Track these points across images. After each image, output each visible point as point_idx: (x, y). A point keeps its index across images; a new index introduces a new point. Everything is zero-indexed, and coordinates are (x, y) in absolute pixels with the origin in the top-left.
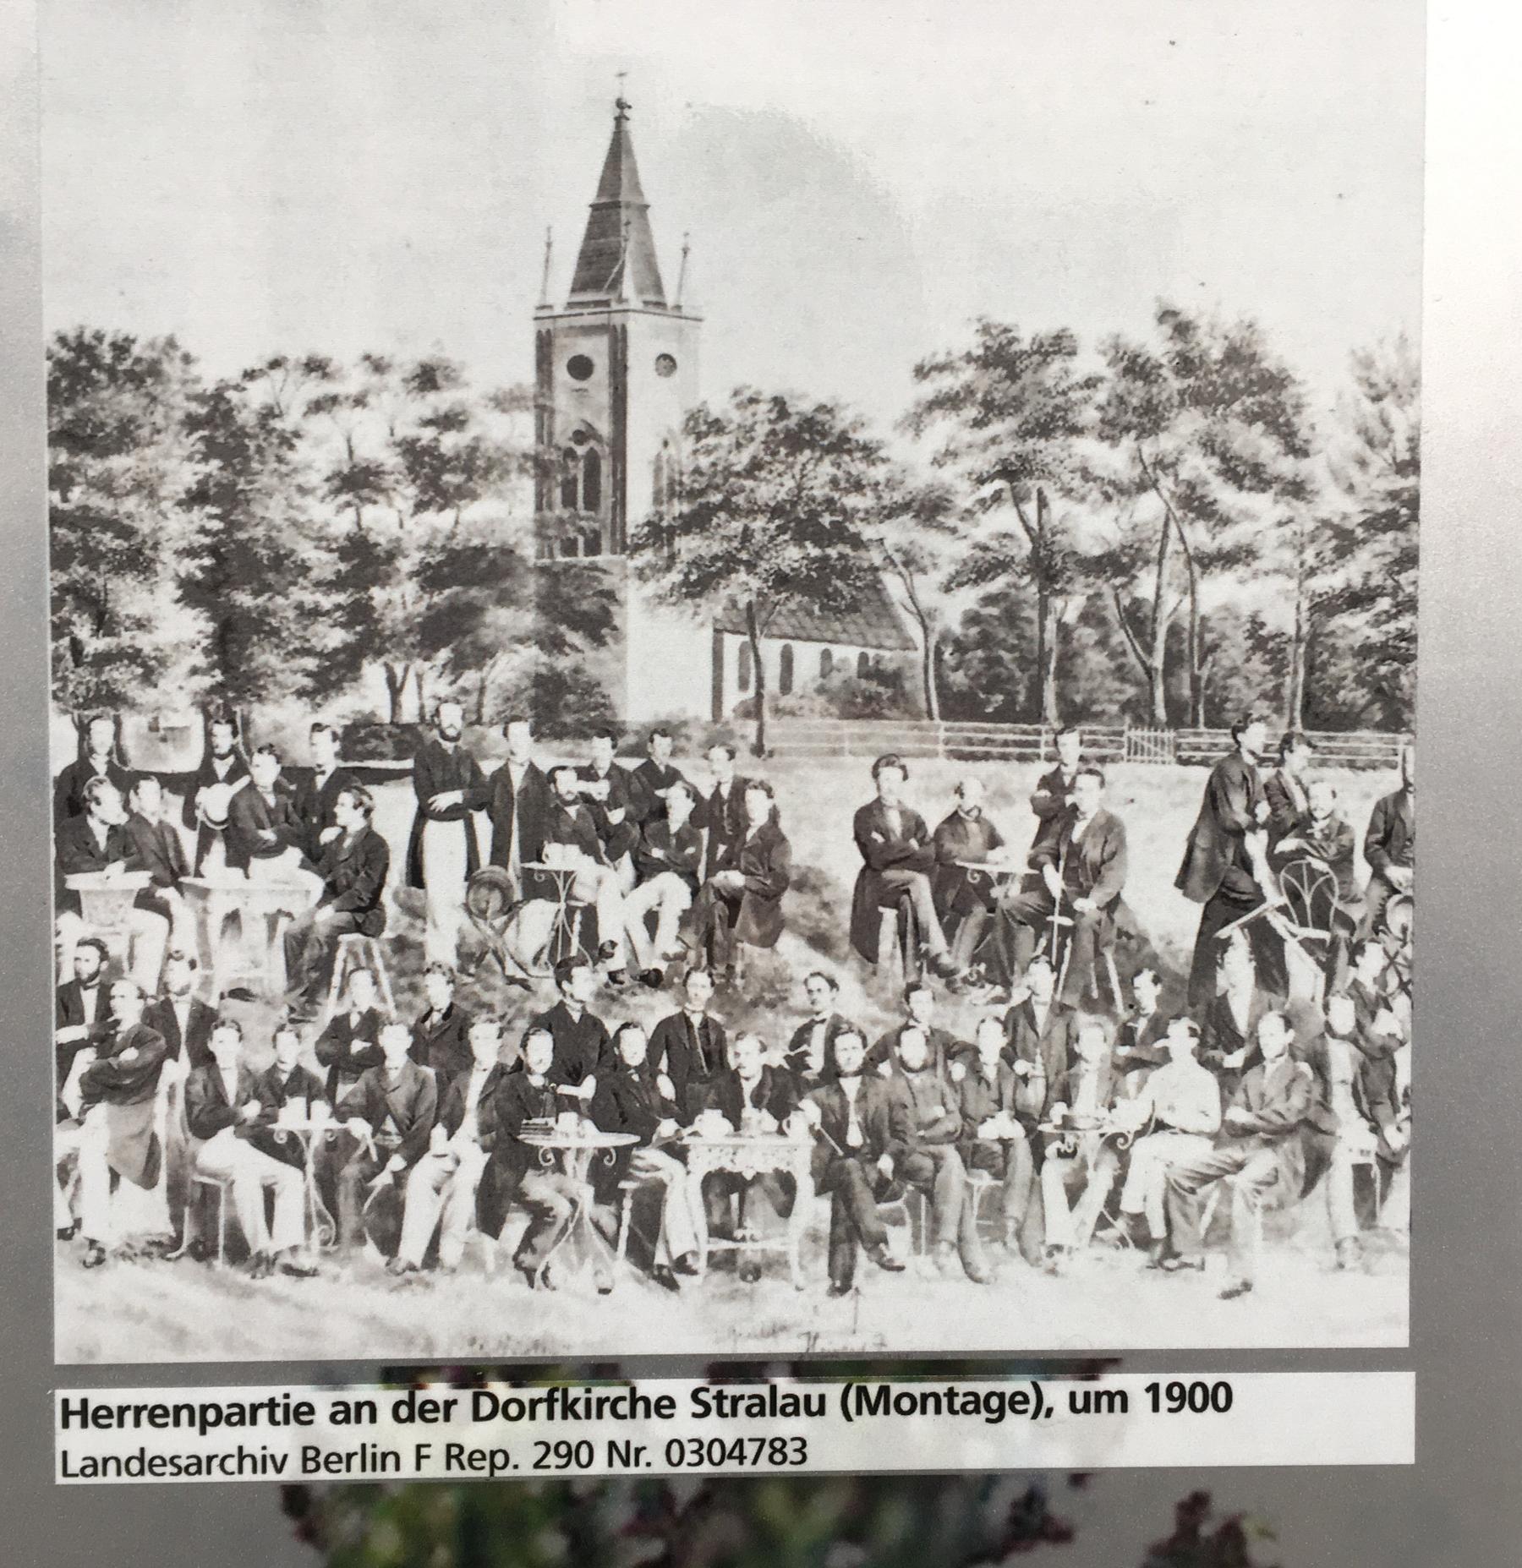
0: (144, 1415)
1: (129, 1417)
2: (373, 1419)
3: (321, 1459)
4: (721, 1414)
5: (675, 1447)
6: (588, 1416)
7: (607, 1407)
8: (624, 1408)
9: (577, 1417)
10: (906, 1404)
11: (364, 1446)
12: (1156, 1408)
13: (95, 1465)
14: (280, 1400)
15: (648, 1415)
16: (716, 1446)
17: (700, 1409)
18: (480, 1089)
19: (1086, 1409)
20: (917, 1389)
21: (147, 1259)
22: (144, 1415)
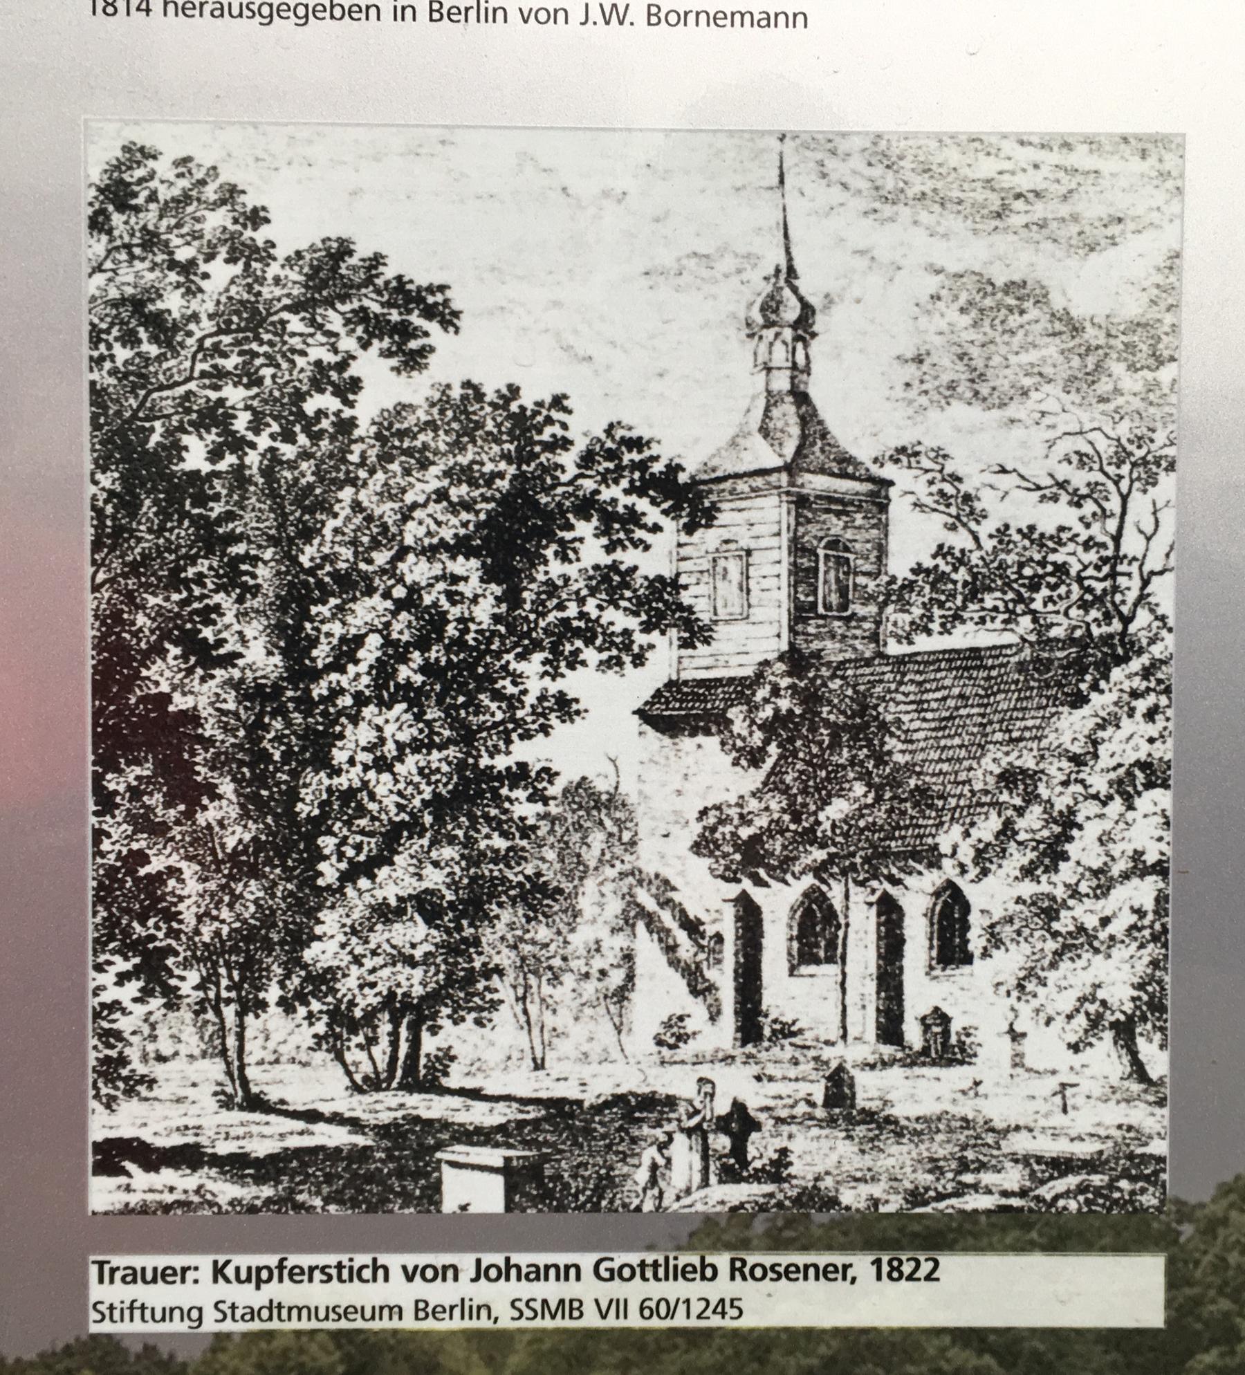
2: (578, 1278)
3: (429, 1310)
6: (667, 1278)
8: (367, 1274)
9: (227, 1281)
10: (758, 1272)
12: (879, 1278)
14: (346, 1263)
15: (817, 1278)
16: (663, 1304)
18: (908, 949)
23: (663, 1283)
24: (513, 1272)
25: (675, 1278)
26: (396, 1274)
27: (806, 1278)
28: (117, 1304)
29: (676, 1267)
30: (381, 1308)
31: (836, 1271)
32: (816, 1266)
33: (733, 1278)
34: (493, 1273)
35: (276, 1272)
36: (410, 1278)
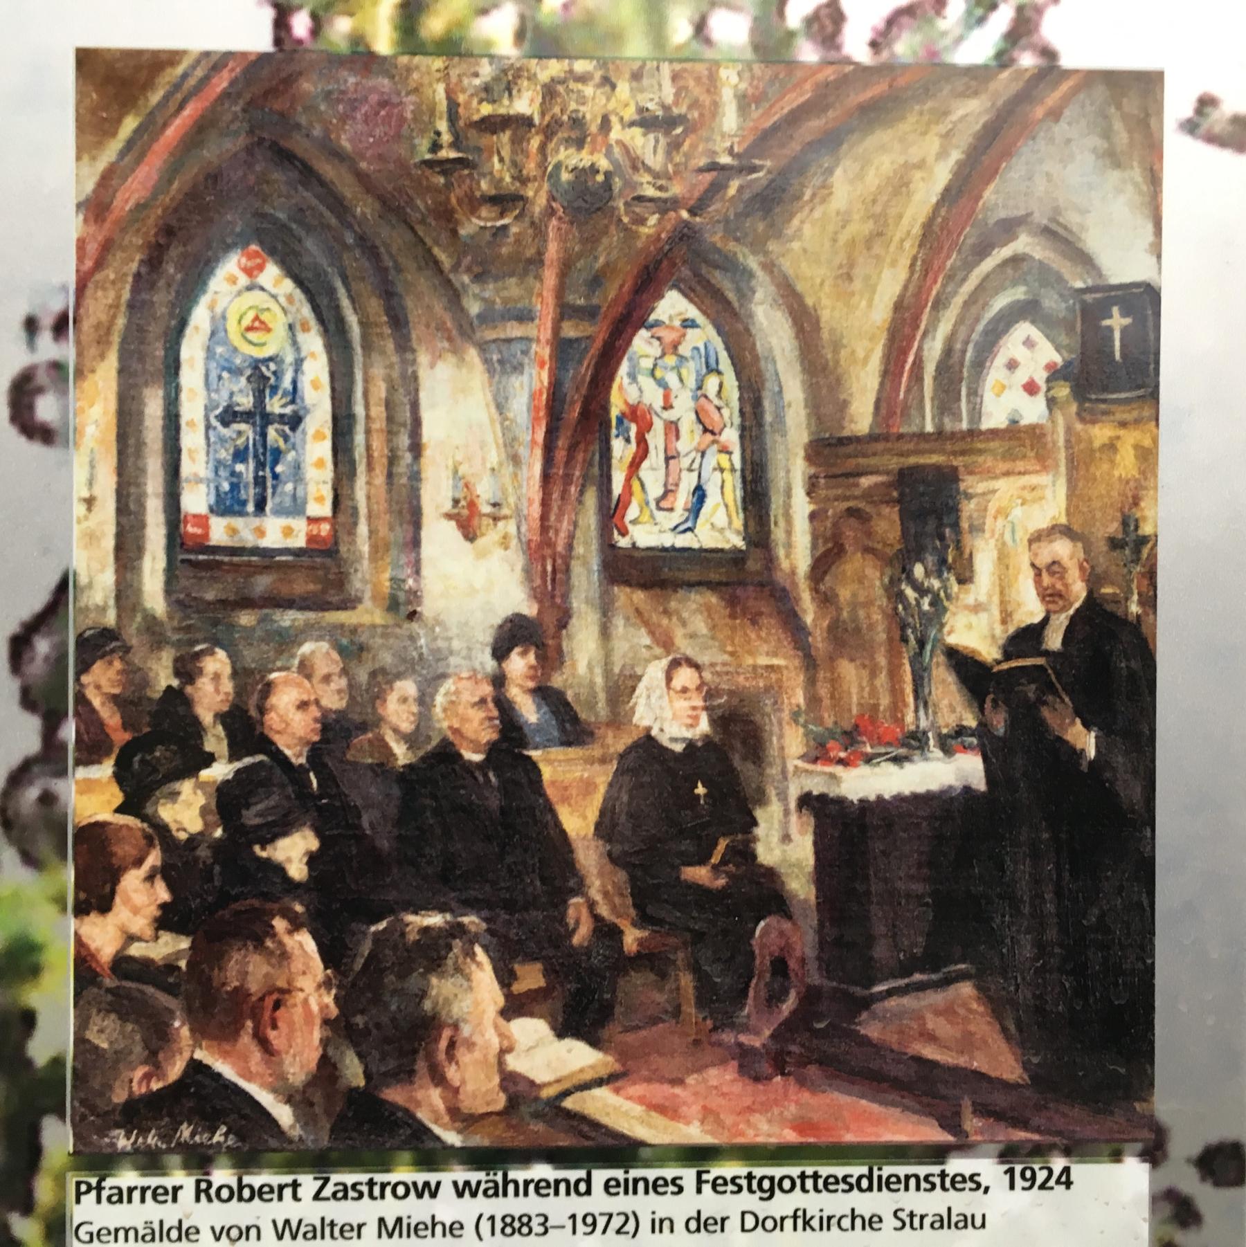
0: (149, 1194)
1: (136, 1195)
12: (1012, 1187)
15: (647, 1192)
20: (902, 1170)
21: (282, 1009)
22: (149, 1194)
23: (379, 1201)
24: (511, 1187)
25: (880, 1189)
26: (447, 1191)
29: (880, 1177)
31: (899, 1181)
32: (646, 1180)
33: (198, 1199)
34: (225, 1193)
36: (460, 1194)
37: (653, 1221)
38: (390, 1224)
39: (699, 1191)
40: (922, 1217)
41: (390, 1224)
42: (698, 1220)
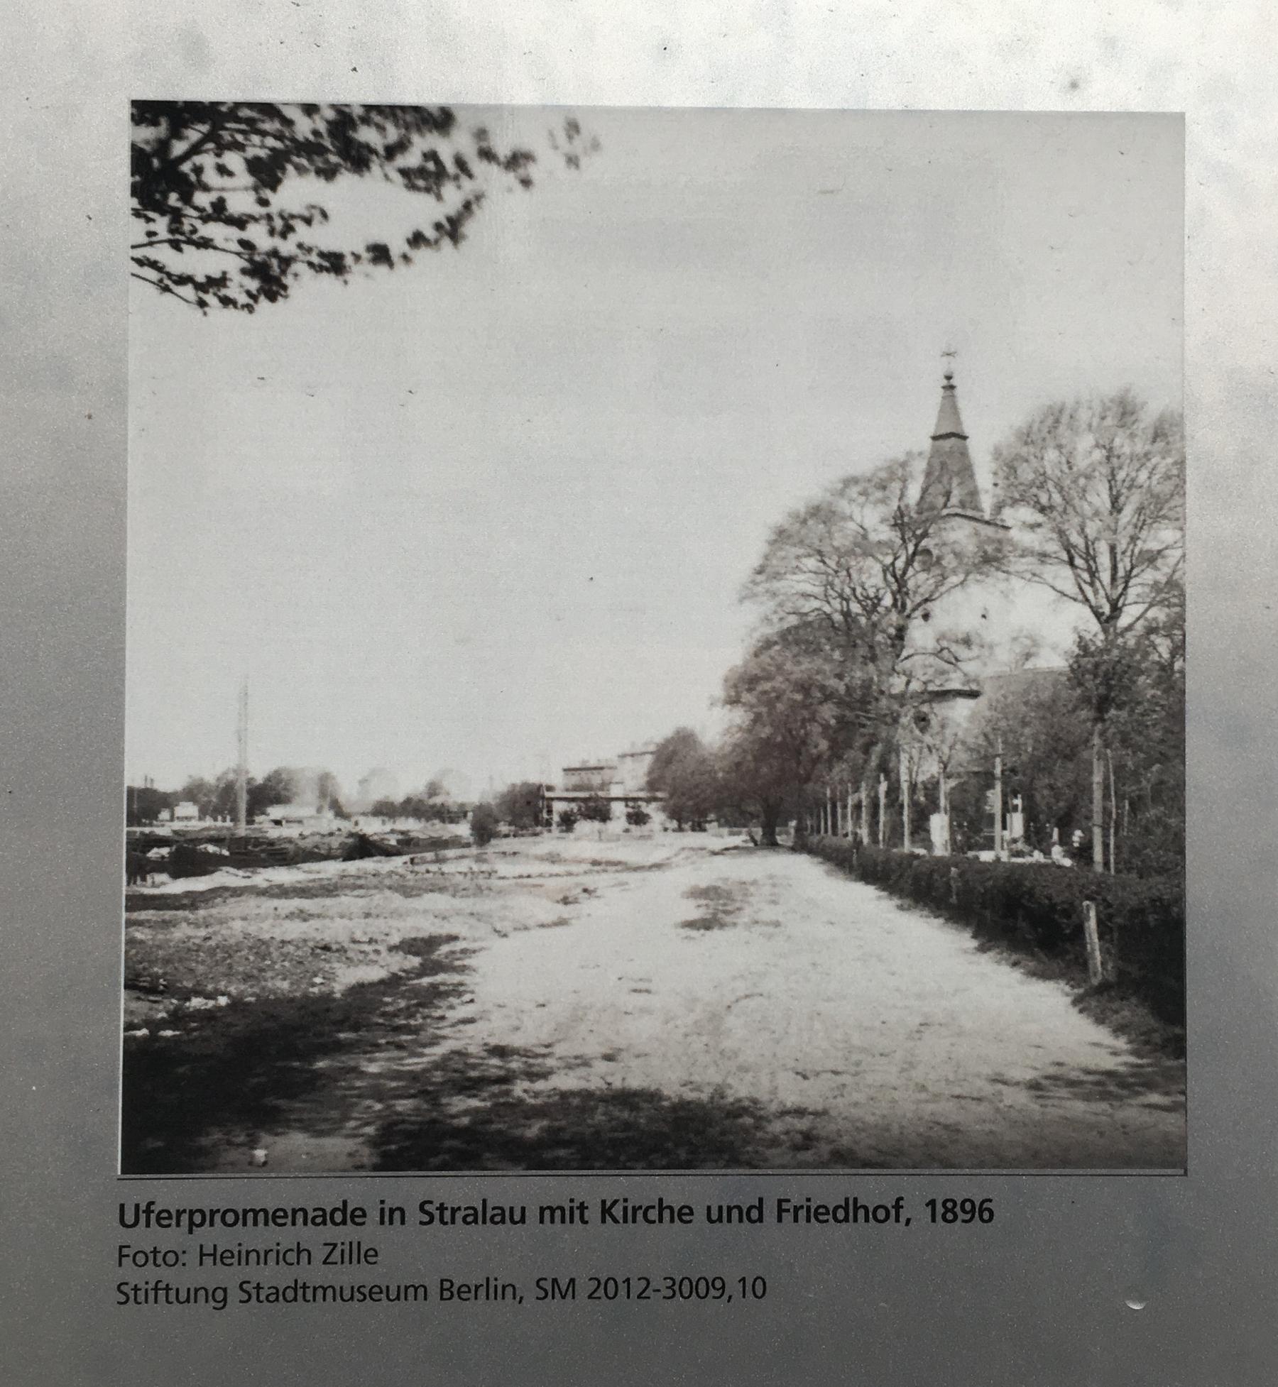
3: (455, 1290)
4: (442, 1222)
5: (759, 1293)
7: (640, 1214)
11: (847, 1200)
13: (324, 1216)
15: (266, 1224)
16: (686, 1282)
17: (426, 1218)
19: (720, 1219)
25: (484, 1222)
27: (294, 1224)
28: (142, 1285)
30: (407, 1288)
33: (604, 1221)
35: (893, 1212)
37: (382, 1210)
38: (564, 1284)
39: (780, 1220)
40: (454, 1211)
41: (564, 1284)
42: (344, 1211)
